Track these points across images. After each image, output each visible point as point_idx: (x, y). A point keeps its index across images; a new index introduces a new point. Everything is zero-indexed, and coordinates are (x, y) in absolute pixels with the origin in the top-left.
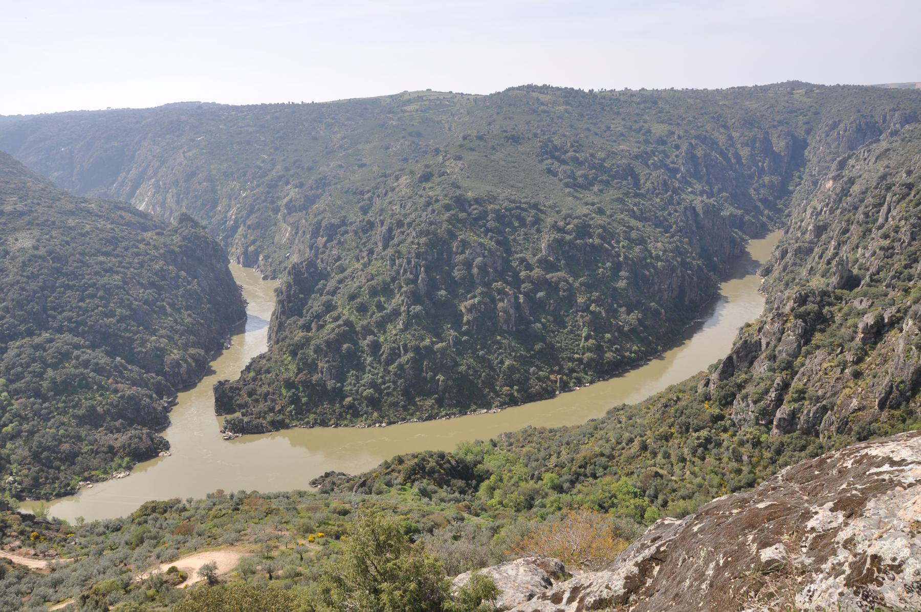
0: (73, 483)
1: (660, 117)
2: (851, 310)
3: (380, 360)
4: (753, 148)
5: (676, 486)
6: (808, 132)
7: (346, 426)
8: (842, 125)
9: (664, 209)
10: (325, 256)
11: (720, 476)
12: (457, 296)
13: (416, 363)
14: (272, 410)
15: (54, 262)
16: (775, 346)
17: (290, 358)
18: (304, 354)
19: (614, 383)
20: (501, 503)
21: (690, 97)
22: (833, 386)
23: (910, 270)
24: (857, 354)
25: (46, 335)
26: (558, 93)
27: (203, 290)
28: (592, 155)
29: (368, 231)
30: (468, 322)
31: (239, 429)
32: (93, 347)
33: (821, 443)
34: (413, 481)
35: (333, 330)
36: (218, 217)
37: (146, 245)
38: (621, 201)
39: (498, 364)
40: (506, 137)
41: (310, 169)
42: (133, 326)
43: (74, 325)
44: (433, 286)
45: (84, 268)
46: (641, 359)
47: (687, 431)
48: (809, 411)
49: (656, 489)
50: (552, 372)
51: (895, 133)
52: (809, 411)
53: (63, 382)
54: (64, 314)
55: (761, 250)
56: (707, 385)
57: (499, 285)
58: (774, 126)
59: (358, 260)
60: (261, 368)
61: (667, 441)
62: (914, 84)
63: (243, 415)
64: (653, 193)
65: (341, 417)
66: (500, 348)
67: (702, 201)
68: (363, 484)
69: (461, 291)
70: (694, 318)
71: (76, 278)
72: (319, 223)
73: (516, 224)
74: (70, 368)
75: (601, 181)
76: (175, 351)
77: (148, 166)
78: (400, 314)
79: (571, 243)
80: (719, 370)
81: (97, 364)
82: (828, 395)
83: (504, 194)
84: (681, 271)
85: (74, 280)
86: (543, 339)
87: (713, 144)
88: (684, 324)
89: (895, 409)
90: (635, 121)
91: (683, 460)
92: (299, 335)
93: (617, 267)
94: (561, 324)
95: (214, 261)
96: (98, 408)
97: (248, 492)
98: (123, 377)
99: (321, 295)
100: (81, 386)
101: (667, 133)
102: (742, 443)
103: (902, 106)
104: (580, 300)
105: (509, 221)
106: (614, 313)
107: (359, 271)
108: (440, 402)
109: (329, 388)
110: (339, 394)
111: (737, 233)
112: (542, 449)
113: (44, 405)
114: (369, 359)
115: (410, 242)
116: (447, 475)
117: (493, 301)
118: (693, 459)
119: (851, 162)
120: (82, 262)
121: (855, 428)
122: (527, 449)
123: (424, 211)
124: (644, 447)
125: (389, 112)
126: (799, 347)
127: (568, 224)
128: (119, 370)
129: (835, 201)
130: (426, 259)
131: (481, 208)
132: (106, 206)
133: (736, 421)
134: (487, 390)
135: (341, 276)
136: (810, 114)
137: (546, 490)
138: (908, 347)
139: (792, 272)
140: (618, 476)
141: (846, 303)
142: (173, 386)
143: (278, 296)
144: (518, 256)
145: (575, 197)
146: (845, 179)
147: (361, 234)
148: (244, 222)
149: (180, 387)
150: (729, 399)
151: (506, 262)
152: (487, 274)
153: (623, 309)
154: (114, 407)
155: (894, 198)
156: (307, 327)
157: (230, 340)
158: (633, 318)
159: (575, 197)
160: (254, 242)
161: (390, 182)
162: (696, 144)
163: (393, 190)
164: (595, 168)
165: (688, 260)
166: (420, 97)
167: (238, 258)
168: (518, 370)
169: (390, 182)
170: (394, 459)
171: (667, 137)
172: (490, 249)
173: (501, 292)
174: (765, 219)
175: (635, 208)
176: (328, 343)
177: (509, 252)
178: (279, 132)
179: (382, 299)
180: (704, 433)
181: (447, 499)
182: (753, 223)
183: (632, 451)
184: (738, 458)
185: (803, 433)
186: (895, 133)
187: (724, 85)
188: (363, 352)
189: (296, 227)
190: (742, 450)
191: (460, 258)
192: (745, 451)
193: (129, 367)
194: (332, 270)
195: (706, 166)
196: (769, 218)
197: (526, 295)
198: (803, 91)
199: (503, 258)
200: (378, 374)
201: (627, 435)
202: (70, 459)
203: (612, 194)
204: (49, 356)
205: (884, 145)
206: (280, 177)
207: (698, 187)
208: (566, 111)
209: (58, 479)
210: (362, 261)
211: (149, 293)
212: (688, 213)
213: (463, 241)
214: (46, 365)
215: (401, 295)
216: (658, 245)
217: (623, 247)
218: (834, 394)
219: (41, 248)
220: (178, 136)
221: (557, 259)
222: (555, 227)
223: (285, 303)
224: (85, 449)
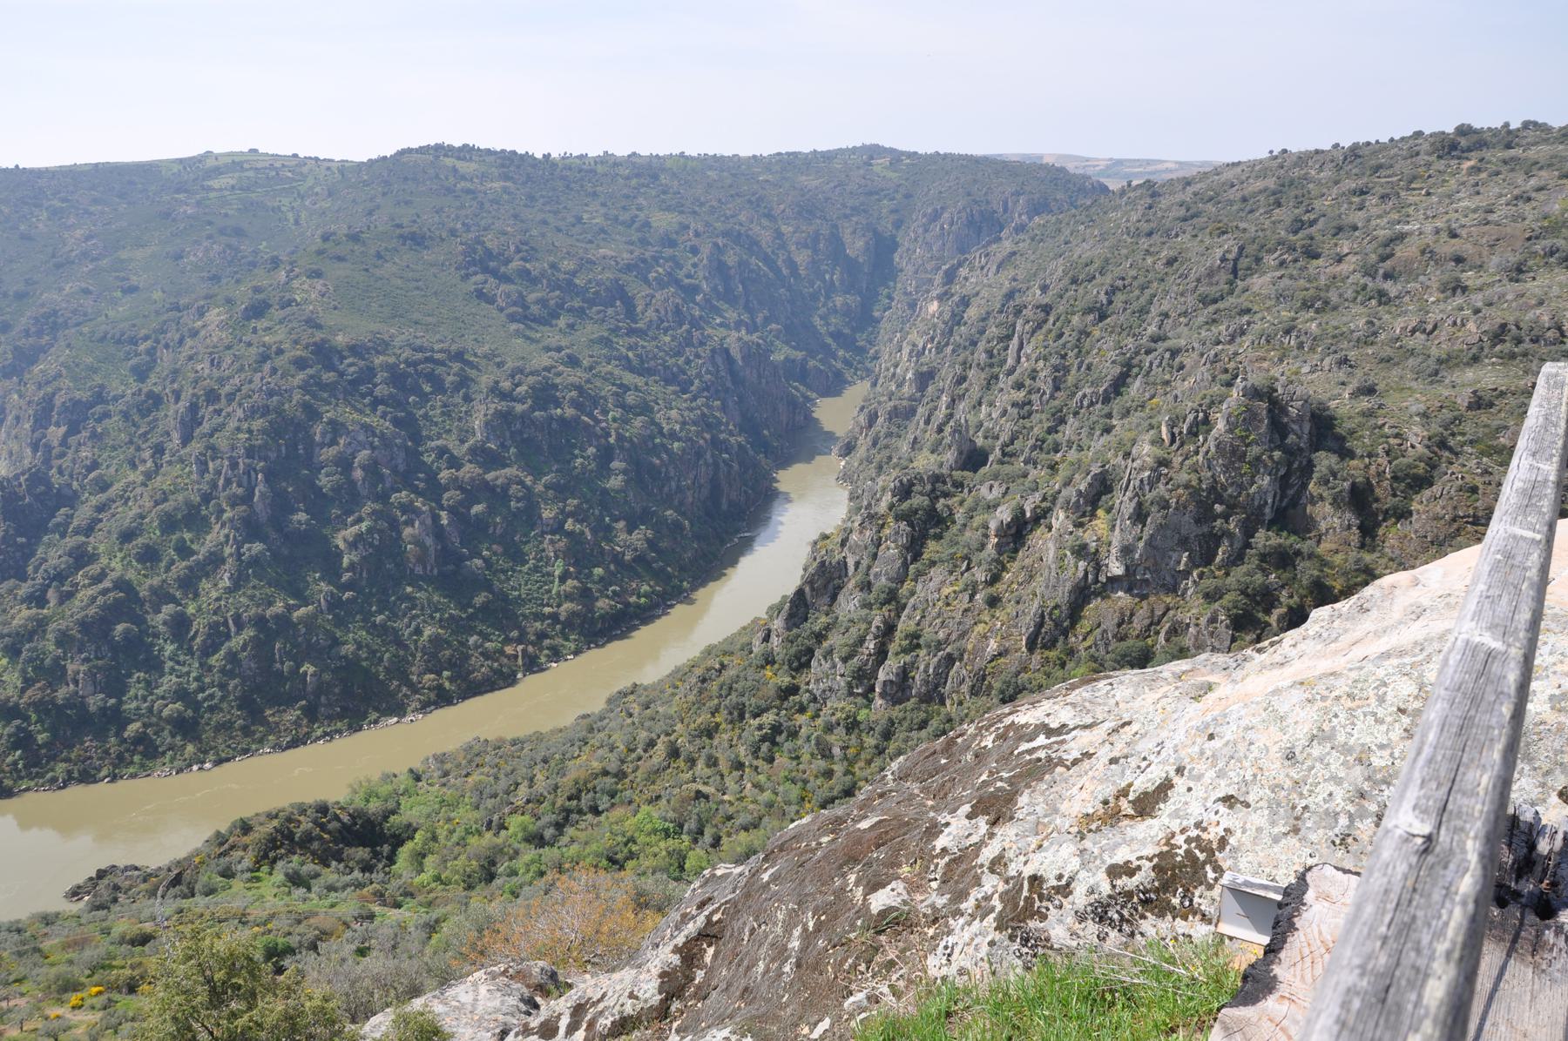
1: (664, 201)
4: (815, 251)
5: (731, 810)
6: (898, 225)
7: (133, 776)
8: (946, 215)
9: (679, 354)
10: (66, 463)
12: (329, 521)
13: (261, 646)
16: (869, 567)
18: (35, 649)
19: (616, 649)
26: (492, 158)
28: (553, 266)
29: (149, 411)
30: (352, 567)
34: (274, 861)
35: (93, 599)
38: (605, 342)
39: (411, 634)
40: (401, 236)
41: (20, 296)
44: (281, 506)
46: (657, 606)
47: (742, 717)
48: (927, 666)
49: (700, 820)
50: (507, 641)
51: (1021, 228)
52: (927, 666)
55: (836, 414)
56: (767, 639)
57: (403, 496)
58: (846, 216)
59: (134, 466)
61: (710, 737)
62: (1041, 157)
65: (121, 760)
67: (740, 339)
68: (177, 881)
69: (335, 512)
70: (738, 531)
72: (48, 401)
73: (427, 388)
75: (569, 310)
78: (223, 561)
79: (523, 417)
80: (784, 614)
82: (953, 637)
83: (403, 339)
84: (713, 456)
86: (488, 586)
87: (753, 245)
88: (723, 542)
90: (624, 208)
91: (739, 766)
92: (22, 615)
93: (606, 455)
94: (518, 557)
99: (63, 536)
102: (829, 728)
103: (1028, 188)
104: (547, 514)
105: (414, 384)
106: (607, 532)
107: (134, 488)
108: (311, 714)
109: (92, 709)
110: (115, 719)
111: (797, 389)
112: (502, 776)
114: (170, 648)
115: (234, 429)
117: (395, 525)
118: (755, 763)
119: (963, 272)
121: (997, 685)
123: (256, 371)
124: (674, 753)
125: (178, 191)
126: (905, 565)
129: (943, 334)
130: (265, 459)
131: (362, 363)
133: (818, 693)
134: (396, 683)
135: (102, 497)
136: (898, 196)
137: (516, 845)
139: (887, 447)
145: (528, 338)
146: (956, 298)
147: (136, 418)
150: (804, 659)
151: (414, 455)
153: (621, 524)
156: (38, 599)
158: (639, 537)
159: (528, 338)
164: (559, 288)
165: (722, 436)
166: (236, 164)
168: (448, 643)
169: (189, 320)
170: (234, 825)
172: (383, 434)
173: (407, 508)
174: (839, 365)
175: (630, 354)
176: (84, 625)
177: (417, 438)
179: (187, 536)
180: (769, 718)
181: (339, 885)
185: (921, 701)
186: (1021, 228)
187: (766, 150)
188: (156, 636)
190: (831, 738)
191: (329, 453)
192: (836, 740)
194: (83, 487)
196: (847, 363)
197: (452, 511)
198: (886, 161)
199: (407, 449)
200: (188, 674)
201: (643, 735)
203: (591, 330)
205: (1007, 246)
207: (732, 315)
210: (141, 468)
212: (719, 360)
213: (331, 422)
215: (223, 526)
217: (614, 420)
221: (502, 445)
222: (495, 390)
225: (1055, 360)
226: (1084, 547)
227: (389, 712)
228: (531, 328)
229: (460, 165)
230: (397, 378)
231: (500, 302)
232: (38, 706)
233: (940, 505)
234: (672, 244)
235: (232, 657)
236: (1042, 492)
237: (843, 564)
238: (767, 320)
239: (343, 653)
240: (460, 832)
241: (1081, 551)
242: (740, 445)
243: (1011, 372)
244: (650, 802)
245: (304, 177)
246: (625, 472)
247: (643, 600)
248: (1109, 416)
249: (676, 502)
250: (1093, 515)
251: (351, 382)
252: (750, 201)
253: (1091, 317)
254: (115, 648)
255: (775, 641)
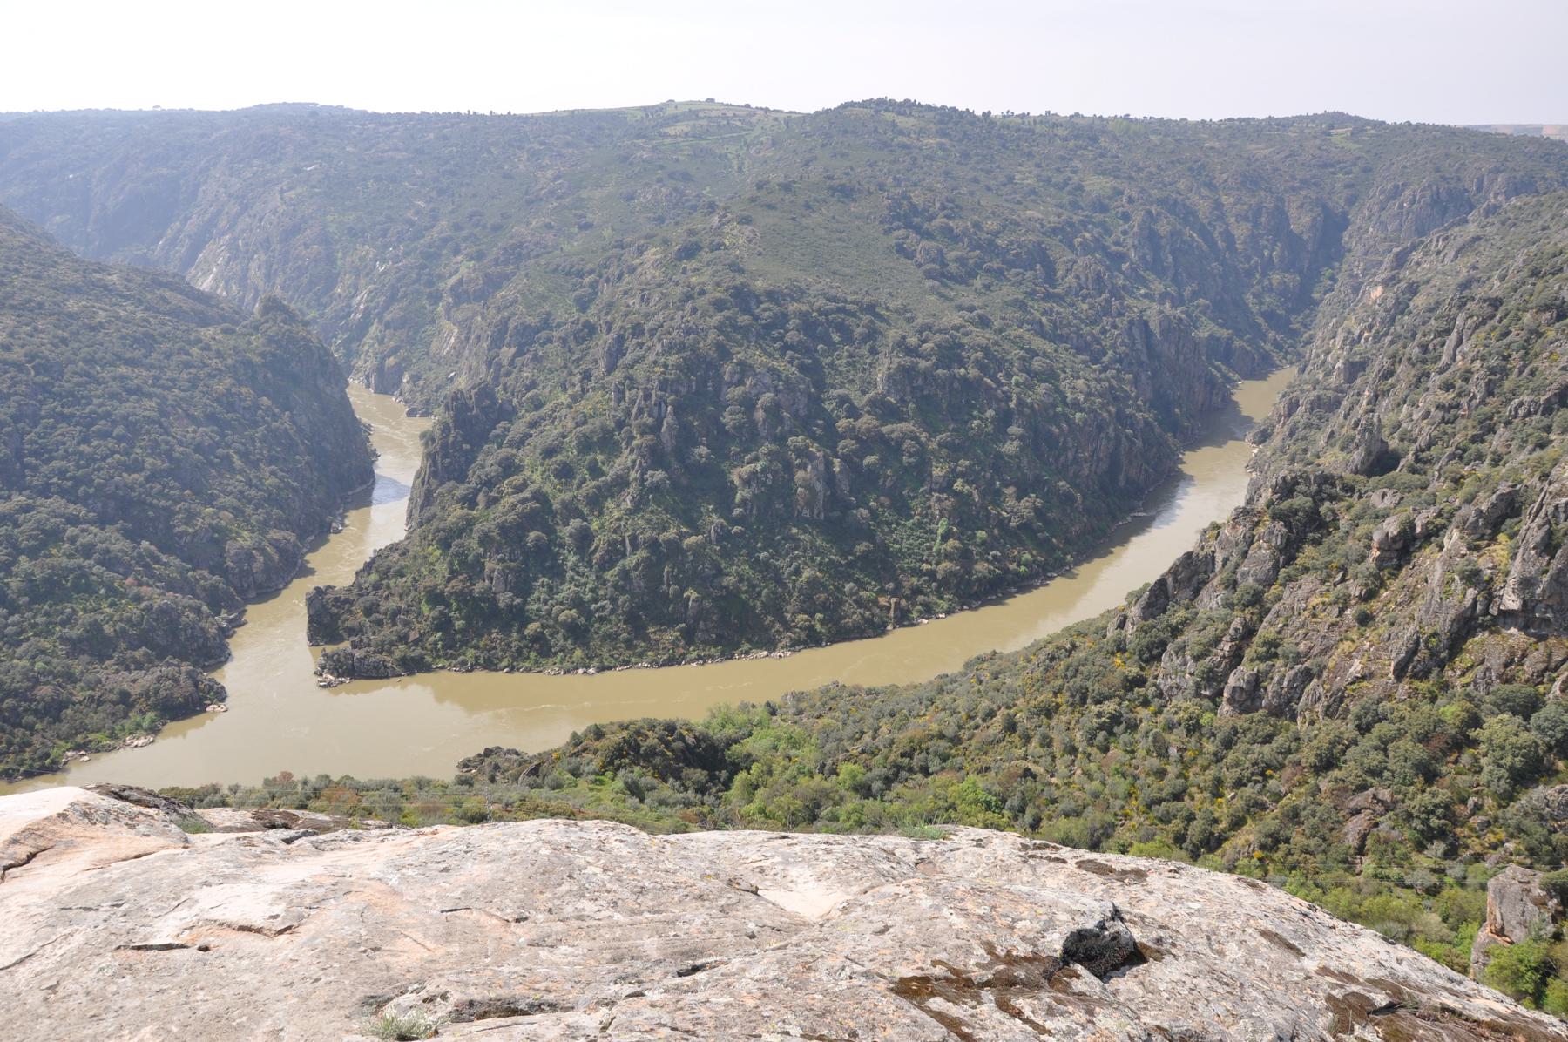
0: (54, 752)
1: (1100, 165)
2: (1367, 508)
3: (590, 562)
4: (1256, 224)
5: (1056, 794)
6: (1351, 201)
7: (528, 670)
8: (1408, 192)
9: (1095, 323)
10: (510, 381)
11: (1130, 779)
12: (727, 457)
13: (651, 568)
14: (403, 639)
15: (37, 374)
16: (1238, 565)
17: (438, 552)
18: (462, 546)
19: (989, 614)
20: (762, 811)
21: (1155, 132)
22: (1324, 637)
23: (1480, 446)
24: (1366, 585)
25: (19, 499)
26: (930, 115)
27: (300, 430)
28: (977, 225)
29: (584, 339)
30: (744, 502)
31: (346, 670)
32: (102, 521)
33: (1298, 732)
34: (618, 769)
35: (514, 506)
36: (336, 305)
37: (203, 349)
38: (1021, 305)
39: (790, 575)
40: (831, 188)
41: (496, 228)
42: (172, 488)
43: (70, 483)
44: (686, 437)
45: (92, 386)
46: (1037, 576)
47: (1083, 701)
48: (1282, 678)
49: (1023, 798)
50: (882, 592)
51: (1492, 211)
52: (1282, 678)
53: (46, 580)
54: (55, 464)
55: (1257, 399)
56: (1121, 625)
57: (799, 440)
58: (1293, 189)
59: (565, 389)
60: (389, 568)
61: (1049, 716)
62: (1540, 128)
63: (354, 646)
64: (1077, 295)
65: (519, 655)
66: (797, 548)
67: (1161, 312)
68: (535, 771)
69: (734, 449)
70: (1132, 510)
71: (77, 402)
72: (504, 323)
73: (836, 338)
74: (59, 557)
75: (988, 271)
76: (246, 534)
77: (219, 212)
78: (628, 484)
79: (927, 375)
80: (1142, 602)
81: (107, 551)
82: (1315, 651)
83: (819, 287)
84: (1115, 430)
85: (73, 405)
86: (871, 537)
87: (1188, 215)
88: (1115, 519)
89: (1421, 679)
90: (1058, 170)
91: (1072, 750)
92: (456, 513)
93: (1005, 419)
94: (903, 510)
95: (321, 382)
96: (106, 627)
97: (335, 778)
98: (152, 576)
99: (500, 447)
100: (77, 588)
101: (1110, 192)
102: (1170, 727)
103: (1510, 165)
104: (938, 472)
105: (824, 333)
106: (995, 496)
107: (564, 408)
108: (689, 636)
109: (501, 605)
110: (519, 616)
111: (1218, 369)
112: (850, 722)
113: (11, 619)
114: (572, 559)
115: (653, 362)
116: (677, 759)
117: (788, 467)
118: (1089, 749)
119: (1416, 256)
120: (87, 374)
121: (1354, 709)
122: (825, 720)
123: (678, 309)
124: (1011, 727)
125: (638, 136)
126: (1276, 568)
127: (924, 342)
128: (146, 565)
129: (1382, 323)
130: (677, 392)
131: (776, 309)
132: (139, 280)
133: (1165, 689)
134: (770, 618)
135: (535, 415)
136: (1356, 170)
137: (843, 792)
138: (1448, 576)
139: (1304, 438)
140: (963, 773)
141: (1360, 497)
142: (239, 593)
143: (426, 445)
144: (835, 392)
145: (942, 296)
146: (1403, 285)
147: (572, 345)
148: (380, 316)
149: (252, 594)
150: (1155, 652)
151: (816, 401)
152: (781, 421)
153: (1011, 490)
154: (133, 625)
155: (1469, 322)
156: (469, 501)
157: (344, 517)
158: (1026, 506)
159: (942, 296)
160: (394, 351)
161: (629, 257)
162: (1159, 214)
163: (632, 270)
164: (980, 247)
165: (1128, 411)
166: (693, 112)
167: (368, 377)
168: (824, 586)
169: (629, 257)
170: (588, 731)
171: (1110, 198)
172: (788, 378)
173: (802, 452)
174: (1268, 347)
175: (1044, 319)
176: (503, 529)
177: (820, 385)
178: (447, 162)
179: (600, 458)
180: (1109, 707)
181: (671, 801)
182: (1247, 352)
183: (992, 731)
184: (1162, 751)
185: (1271, 714)
186: (1492, 211)
187: (1215, 115)
188: (562, 546)
189: (466, 326)
190: (1170, 738)
191: (735, 392)
192: (1175, 739)
193: (164, 558)
194: (521, 404)
195: (1173, 253)
196: (1277, 345)
197: (845, 459)
198: (1346, 131)
199: (809, 395)
200: (585, 584)
201: (985, 704)
202: (54, 710)
203: (1007, 292)
204: (24, 533)
205: (1472, 229)
206: (445, 241)
207: (1158, 287)
208: (941, 146)
209: (29, 744)
210: (570, 392)
211: (206, 434)
212: (1136, 332)
213: (741, 363)
214: (16, 551)
215: (632, 451)
216: (1079, 384)
217: (1017, 384)
218: (1326, 650)
219: (16, 349)
220: (273, 162)
221: (902, 400)
222: (901, 345)
223: (438, 459)
224: (79, 696)
225: (1493, 362)
226: (1477, 572)
227: (760, 645)
228: (945, 285)
229: (900, 120)
230: (808, 325)
231: (919, 258)
232: (459, 595)
233: (1325, 508)
234: (1104, 209)
235: (625, 574)
236: (1438, 506)
237: (1211, 559)
238: (1195, 295)
239: (725, 583)
240: (792, 771)
241: (1472, 577)
242: (1146, 422)
243: (1442, 371)
244: (979, 772)
245: (752, 127)
246: (1021, 438)
247: (1023, 568)
248: (1548, 429)
249: (1071, 474)
250: (1493, 539)
251: (765, 327)
252: (1191, 169)
253: (1547, 315)
254: (527, 553)
255: (1129, 628)
